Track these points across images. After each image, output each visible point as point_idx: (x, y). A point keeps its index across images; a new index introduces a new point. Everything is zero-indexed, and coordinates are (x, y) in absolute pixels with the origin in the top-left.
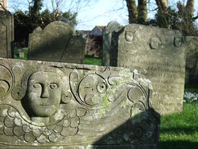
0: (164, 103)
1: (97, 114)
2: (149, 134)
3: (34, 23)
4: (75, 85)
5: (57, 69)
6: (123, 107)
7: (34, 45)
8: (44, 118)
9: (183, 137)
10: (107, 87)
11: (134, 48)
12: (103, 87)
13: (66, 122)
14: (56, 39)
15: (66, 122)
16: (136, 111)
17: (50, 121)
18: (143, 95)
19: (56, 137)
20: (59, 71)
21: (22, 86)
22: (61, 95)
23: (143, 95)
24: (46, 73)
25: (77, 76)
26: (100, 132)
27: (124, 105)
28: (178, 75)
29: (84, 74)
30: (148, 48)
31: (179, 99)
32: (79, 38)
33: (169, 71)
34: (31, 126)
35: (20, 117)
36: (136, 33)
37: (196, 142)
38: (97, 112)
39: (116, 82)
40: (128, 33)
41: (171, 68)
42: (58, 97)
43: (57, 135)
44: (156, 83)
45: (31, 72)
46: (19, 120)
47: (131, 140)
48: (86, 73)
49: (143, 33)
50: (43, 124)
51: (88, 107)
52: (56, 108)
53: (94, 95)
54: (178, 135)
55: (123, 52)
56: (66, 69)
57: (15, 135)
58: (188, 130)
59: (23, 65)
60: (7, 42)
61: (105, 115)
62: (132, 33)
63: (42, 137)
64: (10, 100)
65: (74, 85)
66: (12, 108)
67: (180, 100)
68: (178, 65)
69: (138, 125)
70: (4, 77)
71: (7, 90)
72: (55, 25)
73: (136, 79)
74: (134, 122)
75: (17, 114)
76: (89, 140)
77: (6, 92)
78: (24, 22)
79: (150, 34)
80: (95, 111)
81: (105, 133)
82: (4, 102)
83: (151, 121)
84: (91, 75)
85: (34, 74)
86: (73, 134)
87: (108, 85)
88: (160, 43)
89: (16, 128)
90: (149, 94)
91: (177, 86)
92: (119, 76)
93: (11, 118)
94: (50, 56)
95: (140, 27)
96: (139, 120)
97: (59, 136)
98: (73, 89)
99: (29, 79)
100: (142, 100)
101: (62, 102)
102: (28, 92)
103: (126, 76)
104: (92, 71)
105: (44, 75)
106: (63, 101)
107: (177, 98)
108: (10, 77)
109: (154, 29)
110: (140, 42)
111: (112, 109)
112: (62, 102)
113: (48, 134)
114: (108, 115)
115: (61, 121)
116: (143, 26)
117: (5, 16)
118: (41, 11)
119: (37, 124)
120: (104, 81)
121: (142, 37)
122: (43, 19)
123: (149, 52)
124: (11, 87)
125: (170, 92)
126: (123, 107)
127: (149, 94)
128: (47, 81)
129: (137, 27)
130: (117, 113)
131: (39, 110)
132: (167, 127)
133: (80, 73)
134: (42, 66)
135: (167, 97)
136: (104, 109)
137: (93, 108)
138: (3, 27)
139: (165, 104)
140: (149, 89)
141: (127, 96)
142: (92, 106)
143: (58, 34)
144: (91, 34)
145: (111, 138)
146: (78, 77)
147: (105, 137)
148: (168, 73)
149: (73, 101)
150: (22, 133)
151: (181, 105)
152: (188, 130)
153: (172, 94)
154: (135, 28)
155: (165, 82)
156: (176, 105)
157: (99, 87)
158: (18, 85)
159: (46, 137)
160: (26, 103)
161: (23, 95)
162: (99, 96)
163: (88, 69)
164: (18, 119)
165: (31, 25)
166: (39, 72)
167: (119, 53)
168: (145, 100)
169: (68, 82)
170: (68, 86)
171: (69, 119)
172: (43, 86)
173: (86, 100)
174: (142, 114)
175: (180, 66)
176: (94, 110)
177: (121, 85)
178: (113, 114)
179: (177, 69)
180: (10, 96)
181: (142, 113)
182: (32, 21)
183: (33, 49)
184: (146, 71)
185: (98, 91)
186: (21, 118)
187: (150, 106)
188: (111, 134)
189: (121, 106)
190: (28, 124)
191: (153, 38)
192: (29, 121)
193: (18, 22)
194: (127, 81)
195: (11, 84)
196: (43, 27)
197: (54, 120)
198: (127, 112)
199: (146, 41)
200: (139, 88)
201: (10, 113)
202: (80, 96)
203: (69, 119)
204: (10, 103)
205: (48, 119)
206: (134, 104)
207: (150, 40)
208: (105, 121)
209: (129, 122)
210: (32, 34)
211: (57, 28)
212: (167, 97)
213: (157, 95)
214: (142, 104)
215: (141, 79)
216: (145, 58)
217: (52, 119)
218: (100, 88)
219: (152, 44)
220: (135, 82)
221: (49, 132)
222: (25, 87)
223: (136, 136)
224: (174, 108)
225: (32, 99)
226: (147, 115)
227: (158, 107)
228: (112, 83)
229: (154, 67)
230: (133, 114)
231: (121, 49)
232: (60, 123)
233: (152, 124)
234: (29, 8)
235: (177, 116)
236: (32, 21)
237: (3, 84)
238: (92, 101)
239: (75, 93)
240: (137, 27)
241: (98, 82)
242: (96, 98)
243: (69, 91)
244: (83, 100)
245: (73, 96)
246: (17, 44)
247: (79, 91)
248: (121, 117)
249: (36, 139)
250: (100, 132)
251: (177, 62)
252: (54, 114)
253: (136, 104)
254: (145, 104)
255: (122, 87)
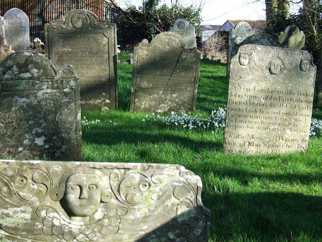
0: (285, 140)
1: (140, 211)
2: (198, 232)
3: (149, 22)
4: (115, 185)
5: (96, 170)
6: (167, 205)
7: (140, 60)
8: (83, 218)
9: (298, 188)
10: (150, 185)
11: (250, 73)
12: (145, 186)
13: (106, 221)
14: (166, 53)
15: (106, 221)
16: (183, 209)
17: (90, 220)
18: (190, 193)
19: (96, 236)
20: (98, 172)
21: (61, 188)
22: (101, 196)
23: (190, 193)
24: (84, 175)
25: (117, 176)
26: (142, 230)
27: (169, 203)
28: (304, 105)
29: (125, 174)
30: (267, 73)
31: (304, 134)
32: (193, 51)
33: (292, 100)
34: (70, 226)
35: (60, 218)
36: (252, 55)
37: (318, 197)
38: (139, 211)
39: (159, 180)
40: (242, 55)
41: (295, 97)
42: (98, 198)
43: (97, 234)
44: (275, 115)
45: (68, 175)
46: (58, 220)
47: (177, 238)
48: (127, 173)
49: (261, 55)
50: (83, 223)
51: (130, 207)
52: (96, 208)
53: (135, 194)
54: (291, 184)
55: (235, 78)
56: (105, 170)
57: (53, 234)
58: (305, 179)
59: (60, 168)
60: (109, 57)
61: (148, 214)
62: (247, 56)
63: (81, 236)
64: (48, 201)
65: (115, 184)
66: (50, 209)
67: (305, 136)
68: (304, 92)
69: (184, 223)
70: (42, 180)
71: (45, 192)
72: (164, 37)
73: (183, 176)
74: (180, 220)
75: (56, 214)
76: (131, 238)
77: (44, 194)
78: (138, 20)
79: (270, 56)
80: (137, 210)
81: (147, 232)
82: (43, 204)
83: (198, 218)
84: (133, 175)
85: (72, 176)
86: (114, 233)
87: (152, 184)
88: (282, 66)
89: (55, 228)
90: (197, 191)
91: (301, 118)
92: (163, 174)
93: (50, 219)
94: (158, 73)
95: (257, 47)
96: (186, 218)
97: (99, 235)
98: (113, 188)
99: (67, 182)
100: (189, 197)
101: (101, 202)
102: (66, 194)
103: (171, 174)
104: (133, 170)
105: (82, 178)
106: (103, 200)
107: (302, 133)
108: (47, 180)
109: (275, 49)
110: (258, 66)
111: (156, 207)
112: (101, 202)
113: (87, 233)
114: (151, 214)
115: (101, 220)
116: (262, 46)
117: (107, 26)
118: (158, 7)
119: (76, 224)
120: (147, 180)
121: (260, 60)
122: (160, 16)
123: (268, 78)
124: (49, 189)
125: (293, 126)
126: (167, 205)
127: (197, 191)
128: (85, 183)
129: (254, 48)
130: (161, 212)
131: (77, 210)
132: (282, 172)
133: (120, 172)
134: (80, 168)
135: (288, 131)
136: (147, 208)
137: (135, 207)
138: (105, 38)
139: (286, 140)
140: (198, 187)
141: (172, 194)
142: (134, 205)
143: (168, 47)
144: (222, 30)
145: (154, 236)
146: (118, 177)
147: (148, 235)
148: (292, 103)
149: (113, 201)
150: (61, 232)
151: (306, 141)
152: (305, 179)
153: (295, 128)
154: (251, 49)
155: (287, 113)
156: (300, 141)
157: (141, 186)
158: (56, 187)
159: (86, 236)
160: (65, 203)
161: (61, 197)
162: (142, 195)
163: (129, 169)
164: (57, 219)
165: (145, 25)
166: (77, 175)
167: (230, 80)
168: (193, 197)
169: (109, 182)
170: (109, 186)
171: (109, 218)
172: (81, 188)
173: (127, 199)
174: (189, 212)
175: (307, 95)
176: (136, 209)
177: (166, 183)
178: (156, 212)
179: (303, 98)
180: (48, 198)
181: (190, 210)
182: (147, 19)
183: (138, 64)
184: (263, 101)
185: (140, 190)
186: (60, 218)
187: (198, 204)
188: (154, 232)
189: (166, 204)
190: (67, 224)
191: (274, 61)
192: (68, 221)
193: (131, 21)
194: (172, 179)
195: (49, 187)
196: (150, 40)
197: (94, 219)
198: (173, 211)
199: (265, 64)
200: (186, 185)
201: (49, 213)
202: (121, 195)
203: (109, 218)
204: (48, 204)
205: (88, 218)
206: (181, 202)
207: (270, 63)
208: (148, 219)
209: (174, 220)
210: (138, 48)
211: (167, 41)
212: (288, 131)
213: (276, 130)
214: (190, 202)
215: (189, 176)
216: (263, 85)
217: (92, 218)
218: (143, 187)
219: (272, 68)
220: (182, 179)
221: (88, 231)
222: (63, 189)
223: (182, 235)
224: (297, 145)
225: (70, 200)
226: (195, 213)
227: (277, 144)
228: (156, 181)
229: (273, 96)
230: (179, 212)
231: (234, 74)
232: (100, 222)
233: (201, 222)
234: (143, 4)
235: (301, 157)
236: (147, 19)
237: (41, 187)
238: (133, 200)
239: (116, 192)
240: (254, 48)
241: (141, 181)
242: (138, 197)
243: (110, 190)
244: (124, 199)
245: (114, 196)
246: (129, 47)
247: (120, 191)
248: (165, 216)
249: (75, 238)
250: (142, 230)
251: (302, 90)
252: (94, 213)
253: (183, 201)
254: (193, 202)
255: (166, 185)
